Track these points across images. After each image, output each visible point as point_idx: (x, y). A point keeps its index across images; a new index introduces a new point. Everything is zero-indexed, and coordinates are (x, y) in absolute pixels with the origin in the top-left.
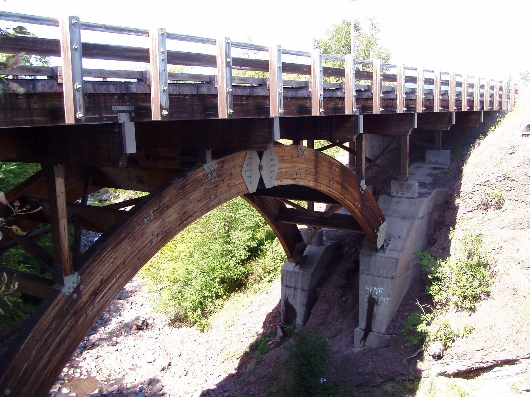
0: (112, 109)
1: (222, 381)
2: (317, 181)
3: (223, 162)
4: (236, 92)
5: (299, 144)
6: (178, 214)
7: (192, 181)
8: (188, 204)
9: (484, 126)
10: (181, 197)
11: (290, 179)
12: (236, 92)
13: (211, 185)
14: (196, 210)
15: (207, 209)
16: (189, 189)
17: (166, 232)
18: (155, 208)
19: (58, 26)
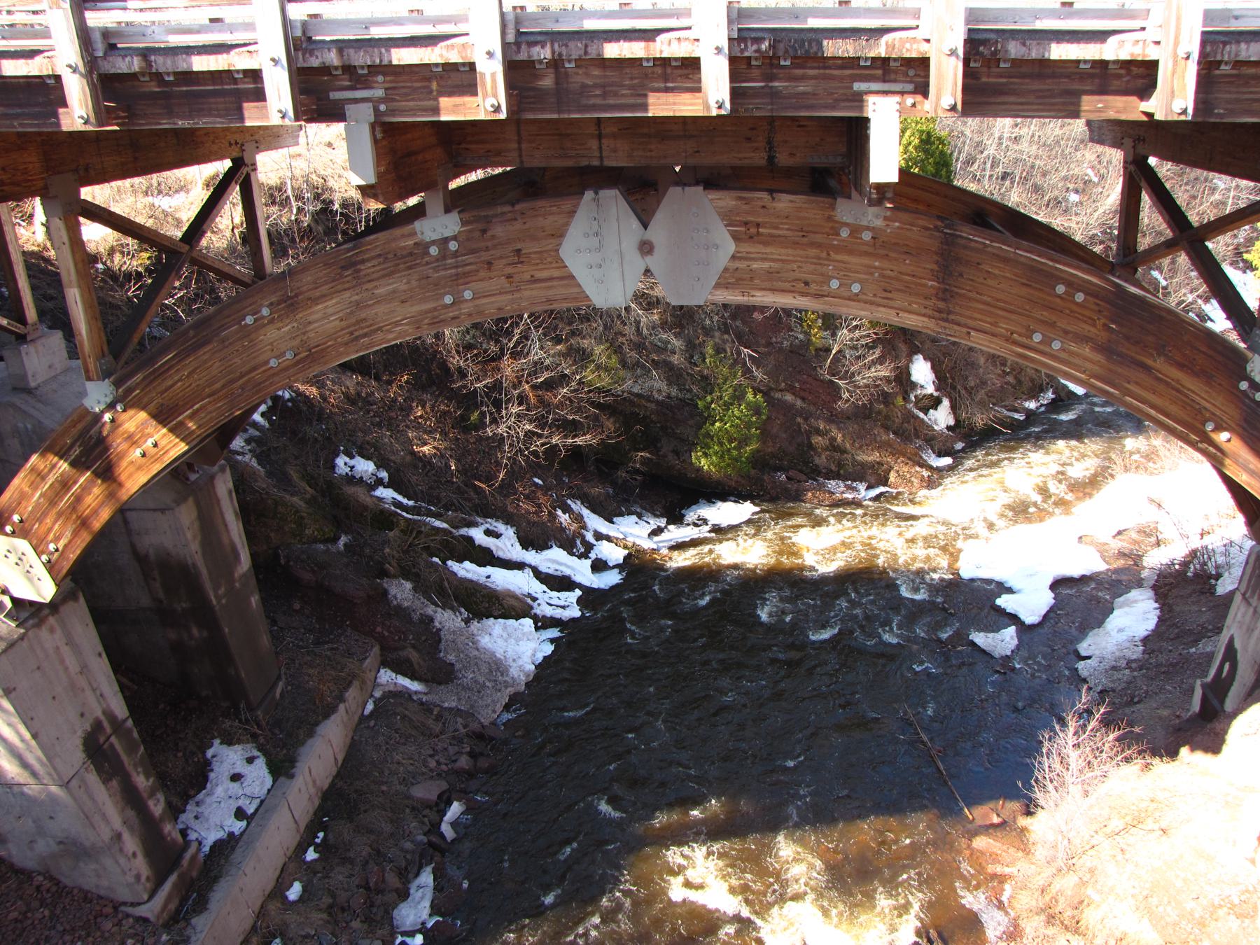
0: (503, 115)
1: (1225, 732)
2: (952, 317)
3: (488, 220)
4: (174, 62)
5: (705, 189)
6: (342, 320)
7: (380, 255)
8: (372, 302)
9: (82, 715)
10: (347, 286)
11: (793, 292)
12: (174, 62)
13: (446, 269)
14: (398, 319)
15: (434, 323)
16: (372, 270)
17: (310, 350)
18: (274, 299)
19: (920, 9)
